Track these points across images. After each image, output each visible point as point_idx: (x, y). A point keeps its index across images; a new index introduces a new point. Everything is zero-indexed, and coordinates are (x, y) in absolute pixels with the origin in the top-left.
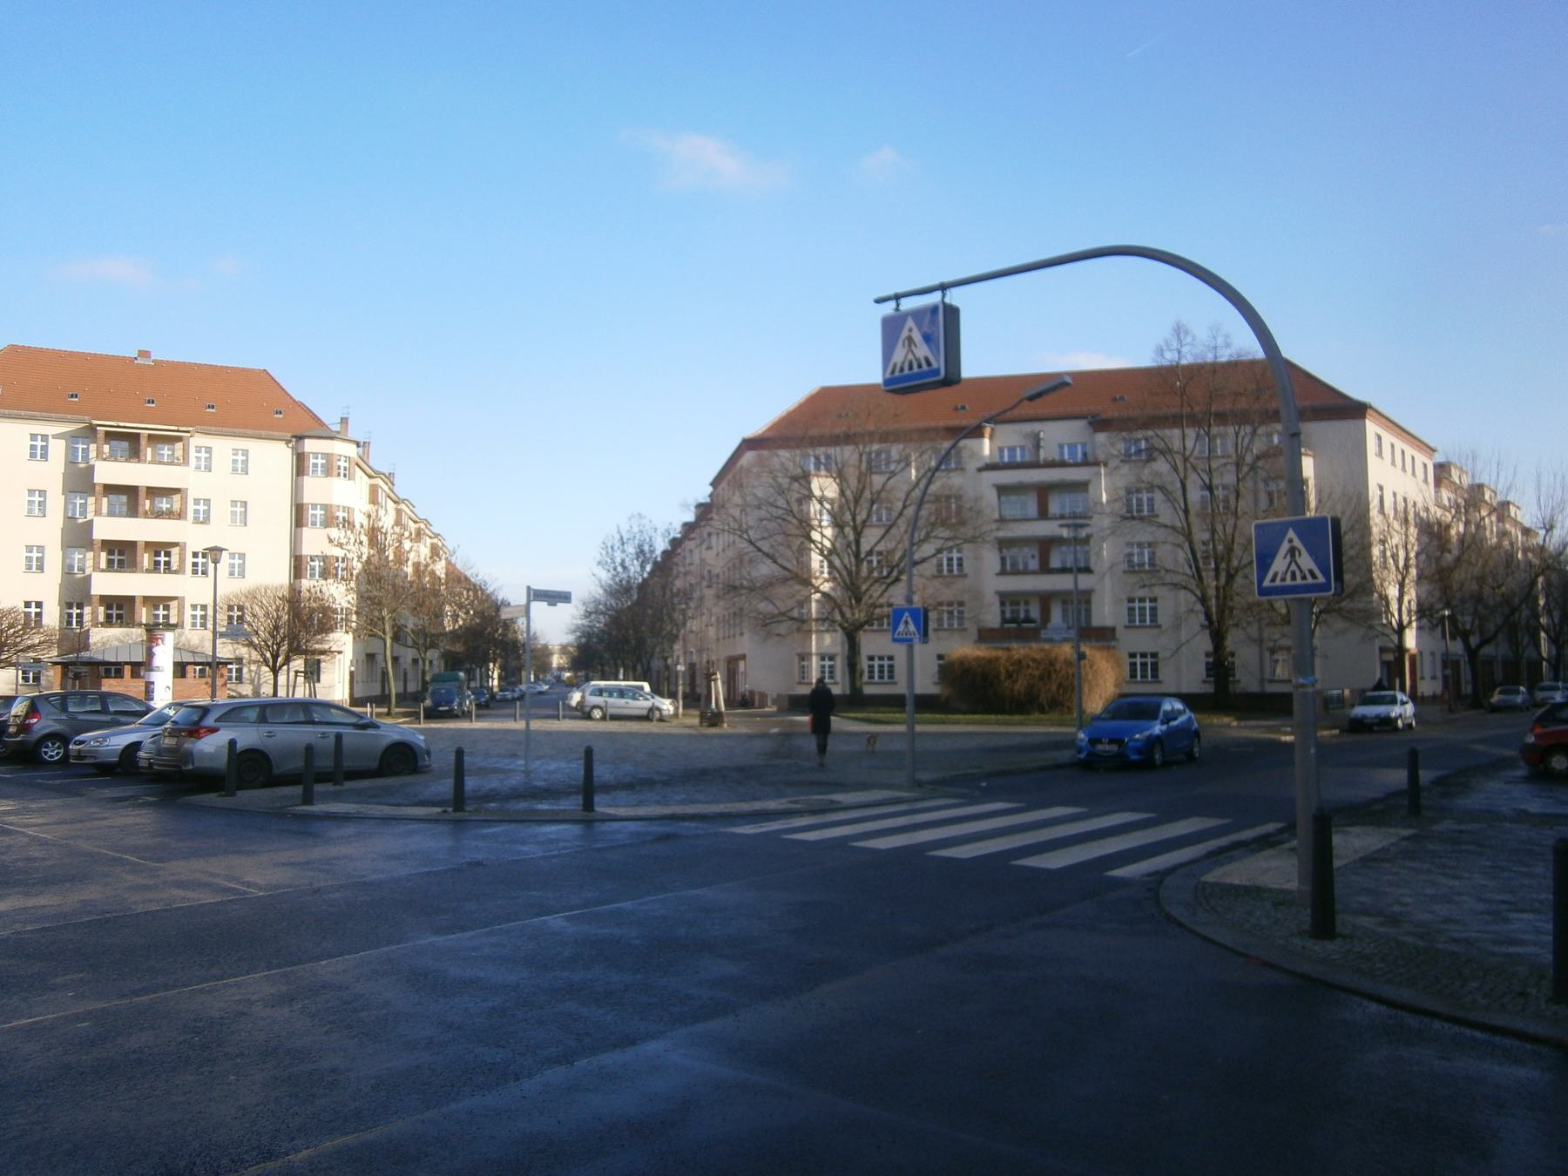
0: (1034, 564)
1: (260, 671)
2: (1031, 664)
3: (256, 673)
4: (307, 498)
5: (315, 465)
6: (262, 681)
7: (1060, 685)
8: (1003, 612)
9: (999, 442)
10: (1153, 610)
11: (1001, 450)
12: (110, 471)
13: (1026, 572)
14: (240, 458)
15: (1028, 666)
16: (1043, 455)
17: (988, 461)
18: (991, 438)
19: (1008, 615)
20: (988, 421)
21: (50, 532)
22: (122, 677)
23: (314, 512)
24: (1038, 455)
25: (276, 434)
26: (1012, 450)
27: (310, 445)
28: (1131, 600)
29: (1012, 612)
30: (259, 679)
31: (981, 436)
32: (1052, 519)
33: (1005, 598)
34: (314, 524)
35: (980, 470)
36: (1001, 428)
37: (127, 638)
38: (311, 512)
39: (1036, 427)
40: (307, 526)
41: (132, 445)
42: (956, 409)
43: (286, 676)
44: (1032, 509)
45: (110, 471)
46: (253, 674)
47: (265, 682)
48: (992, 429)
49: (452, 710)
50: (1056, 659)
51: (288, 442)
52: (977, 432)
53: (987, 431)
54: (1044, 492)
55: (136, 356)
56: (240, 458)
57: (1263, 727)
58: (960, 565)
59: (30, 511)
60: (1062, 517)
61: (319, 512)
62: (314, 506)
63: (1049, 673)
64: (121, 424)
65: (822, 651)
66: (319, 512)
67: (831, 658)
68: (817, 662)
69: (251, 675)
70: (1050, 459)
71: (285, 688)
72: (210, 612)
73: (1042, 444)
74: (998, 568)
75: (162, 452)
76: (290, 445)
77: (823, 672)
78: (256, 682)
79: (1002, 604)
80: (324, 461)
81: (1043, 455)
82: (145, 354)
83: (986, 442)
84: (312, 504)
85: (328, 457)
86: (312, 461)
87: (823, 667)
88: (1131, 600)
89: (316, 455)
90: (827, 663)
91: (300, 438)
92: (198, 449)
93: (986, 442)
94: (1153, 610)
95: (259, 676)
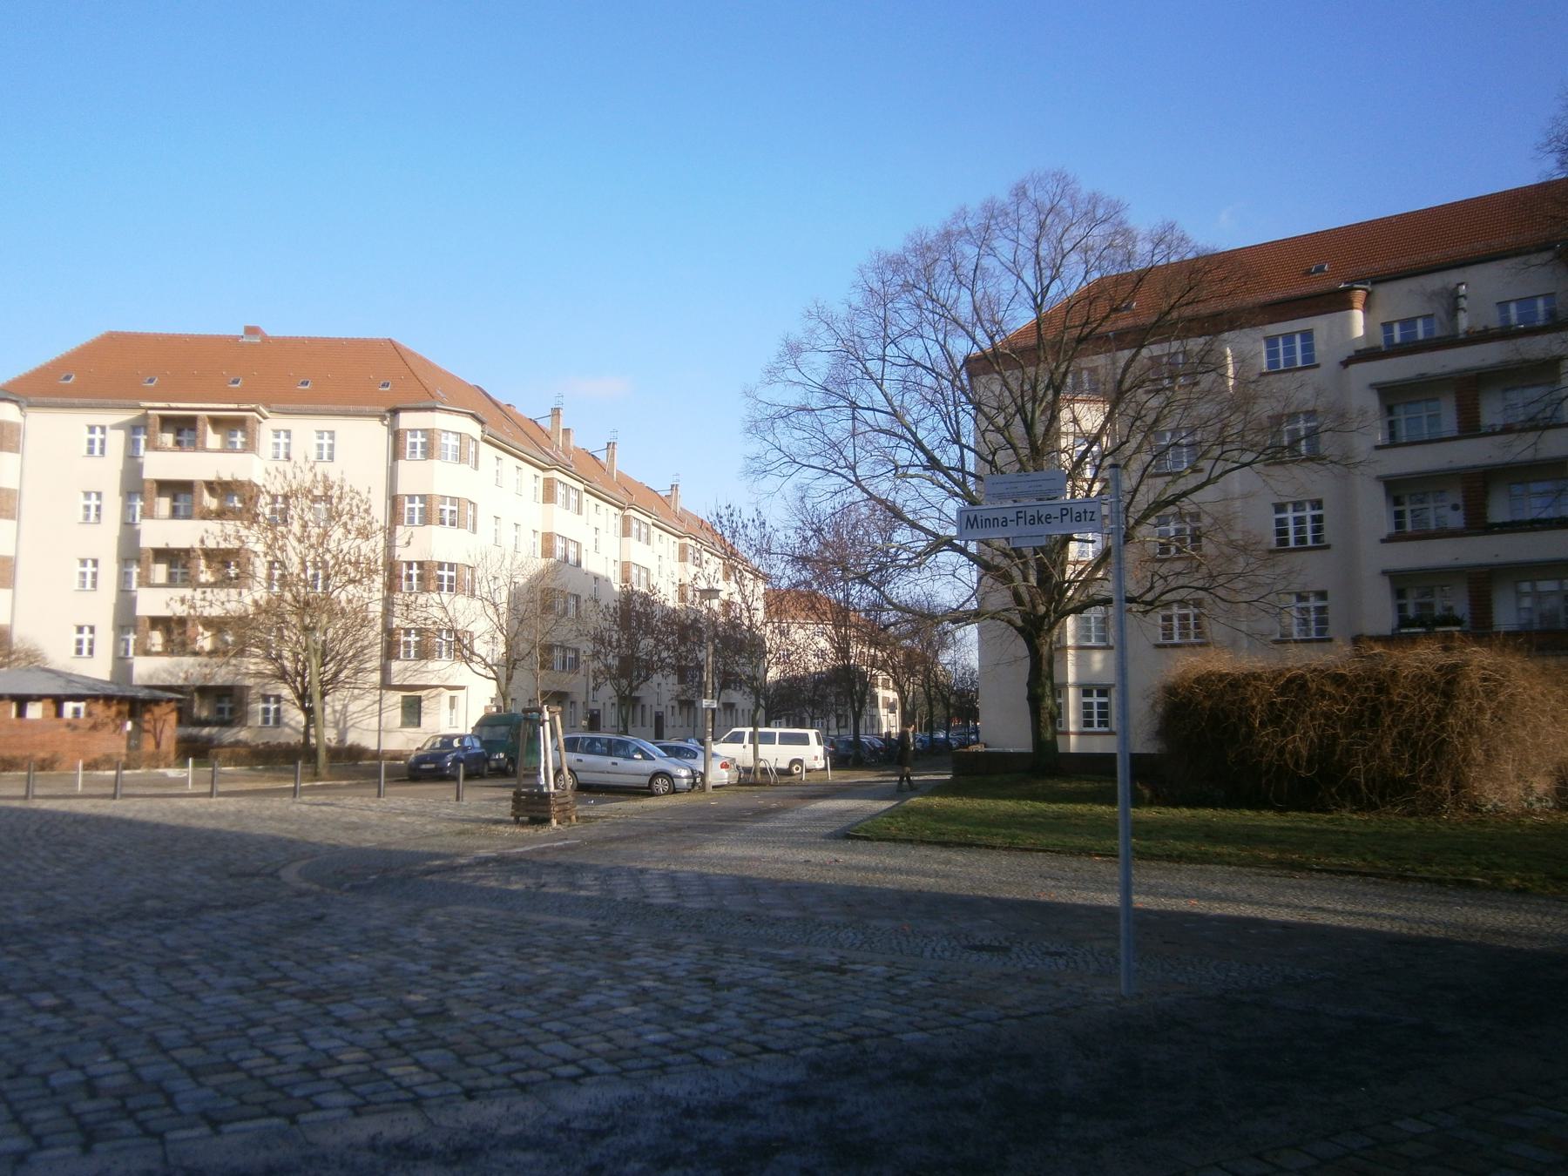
0: (1456, 520)
1: (346, 712)
2: (1329, 688)
3: (341, 714)
4: (402, 490)
5: (414, 445)
6: (349, 724)
7: (1404, 738)
8: (1401, 608)
9: (1382, 316)
10: (1317, 519)
11: (1387, 327)
12: (164, 463)
13: (1443, 533)
14: (326, 441)
15: (1323, 694)
16: (1464, 322)
17: (1362, 346)
18: (1367, 308)
19: (1411, 612)
20: (1363, 281)
21: (105, 541)
22: (808, 744)
23: (411, 506)
24: (1455, 325)
25: (367, 408)
26: (1407, 323)
27: (407, 420)
28: (1280, 508)
29: (1420, 606)
30: (345, 722)
31: (1348, 305)
32: (1486, 434)
33: (1400, 582)
34: (411, 520)
35: (1346, 363)
36: (1382, 290)
37: (177, 669)
38: (407, 505)
39: (1451, 278)
40: (402, 524)
41: (183, 428)
42: (1308, 272)
43: (377, 718)
44: (1448, 415)
45: (164, 463)
46: (338, 715)
47: (352, 726)
48: (1369, 294)
49: (443, 768)
50: (1393, 675)
51: (383, 418)
52: (1338, 301)
53: (1359, 296)
54: (1469, 387)
55: (242, 334)
56: (326, 441)
57: (1252, 837)
58: (1317, 529)
59: (87, 517)
60: (1507, 430)
61: (417, 505)
62: (412, 498)
63: (1376, 711)
64: (173, 405)
65: (1086, 680)
66: (417, 505)
67: (1103, 692)
68: (1078, 700)
69: (335, 716)
70: (1480, 328)
71: (377, 733)
72: (1114, 699)
73: (1463, 303)
74: (1388, 528)
75: (234, 439)
76: (386, 422)
77: (1089, 715)
78: (341, 726)
79: (1399, 593)
80: (424, 440)
81: (1464, 322)
82: (251, 331)
83: (1358, 316)
84: (408, 496)
85: (428, 433)
86: (409, 440)
87: (1088, 706)
88: (1280, 508)
89: (414, 431)
90: (1095, 700)
91: (395, 412)
92: (277, 433)
93: (1358, 316)
94: (1317, 519)
95: (346, 718)
